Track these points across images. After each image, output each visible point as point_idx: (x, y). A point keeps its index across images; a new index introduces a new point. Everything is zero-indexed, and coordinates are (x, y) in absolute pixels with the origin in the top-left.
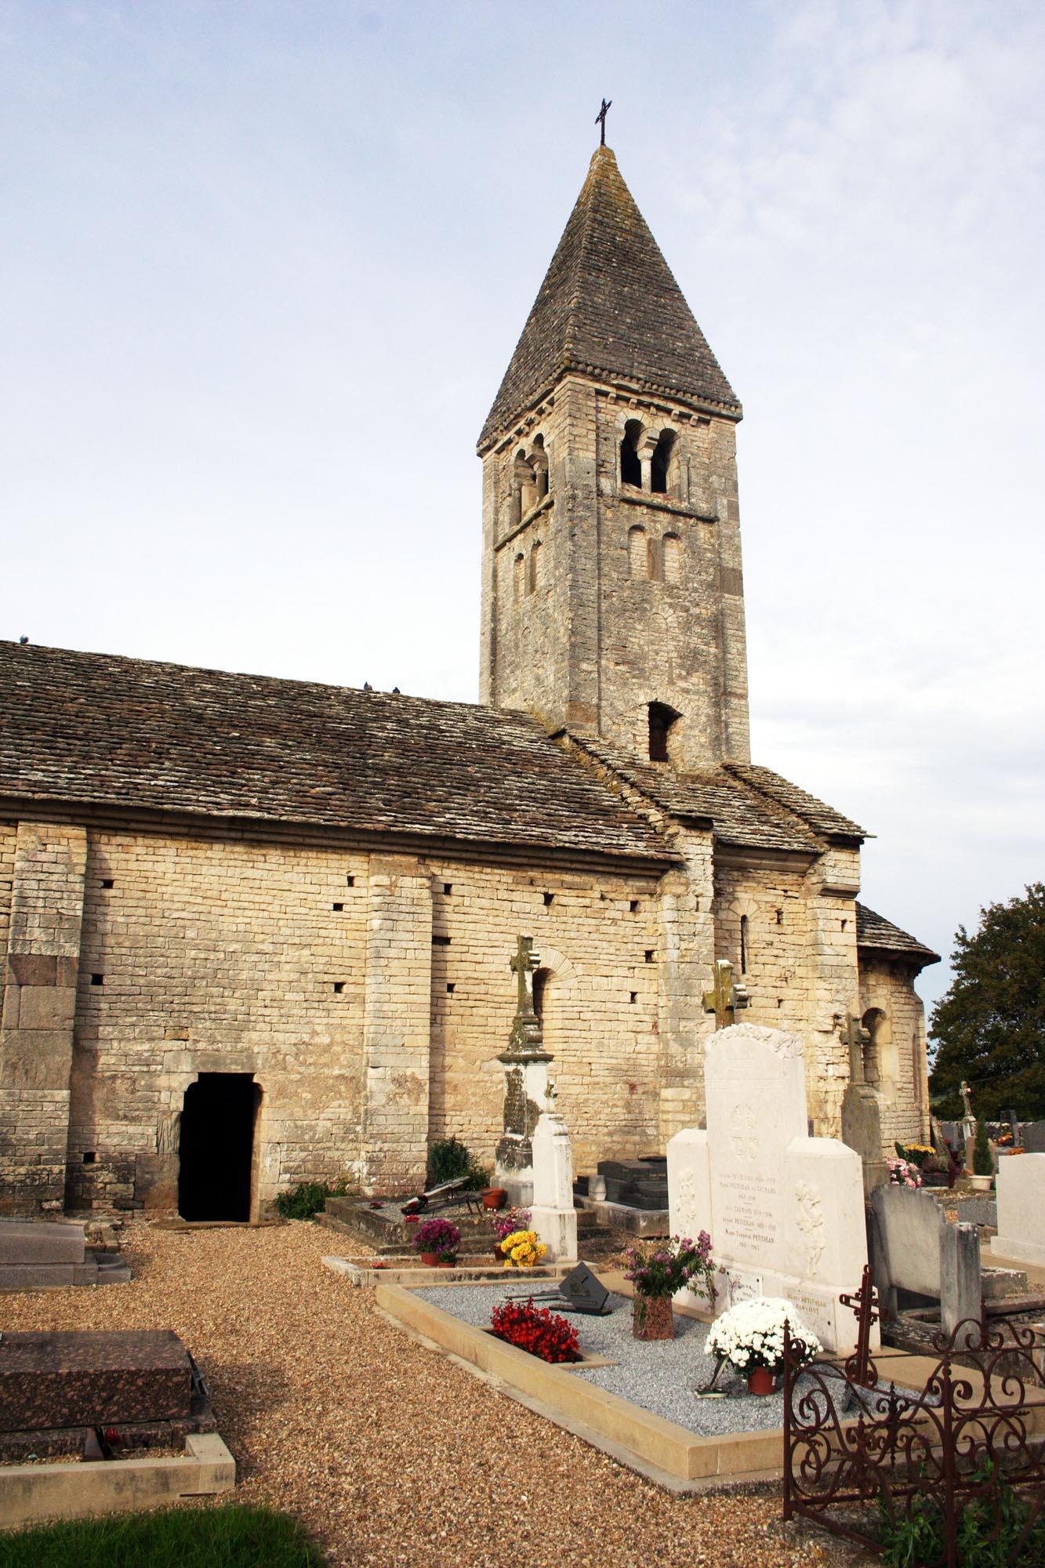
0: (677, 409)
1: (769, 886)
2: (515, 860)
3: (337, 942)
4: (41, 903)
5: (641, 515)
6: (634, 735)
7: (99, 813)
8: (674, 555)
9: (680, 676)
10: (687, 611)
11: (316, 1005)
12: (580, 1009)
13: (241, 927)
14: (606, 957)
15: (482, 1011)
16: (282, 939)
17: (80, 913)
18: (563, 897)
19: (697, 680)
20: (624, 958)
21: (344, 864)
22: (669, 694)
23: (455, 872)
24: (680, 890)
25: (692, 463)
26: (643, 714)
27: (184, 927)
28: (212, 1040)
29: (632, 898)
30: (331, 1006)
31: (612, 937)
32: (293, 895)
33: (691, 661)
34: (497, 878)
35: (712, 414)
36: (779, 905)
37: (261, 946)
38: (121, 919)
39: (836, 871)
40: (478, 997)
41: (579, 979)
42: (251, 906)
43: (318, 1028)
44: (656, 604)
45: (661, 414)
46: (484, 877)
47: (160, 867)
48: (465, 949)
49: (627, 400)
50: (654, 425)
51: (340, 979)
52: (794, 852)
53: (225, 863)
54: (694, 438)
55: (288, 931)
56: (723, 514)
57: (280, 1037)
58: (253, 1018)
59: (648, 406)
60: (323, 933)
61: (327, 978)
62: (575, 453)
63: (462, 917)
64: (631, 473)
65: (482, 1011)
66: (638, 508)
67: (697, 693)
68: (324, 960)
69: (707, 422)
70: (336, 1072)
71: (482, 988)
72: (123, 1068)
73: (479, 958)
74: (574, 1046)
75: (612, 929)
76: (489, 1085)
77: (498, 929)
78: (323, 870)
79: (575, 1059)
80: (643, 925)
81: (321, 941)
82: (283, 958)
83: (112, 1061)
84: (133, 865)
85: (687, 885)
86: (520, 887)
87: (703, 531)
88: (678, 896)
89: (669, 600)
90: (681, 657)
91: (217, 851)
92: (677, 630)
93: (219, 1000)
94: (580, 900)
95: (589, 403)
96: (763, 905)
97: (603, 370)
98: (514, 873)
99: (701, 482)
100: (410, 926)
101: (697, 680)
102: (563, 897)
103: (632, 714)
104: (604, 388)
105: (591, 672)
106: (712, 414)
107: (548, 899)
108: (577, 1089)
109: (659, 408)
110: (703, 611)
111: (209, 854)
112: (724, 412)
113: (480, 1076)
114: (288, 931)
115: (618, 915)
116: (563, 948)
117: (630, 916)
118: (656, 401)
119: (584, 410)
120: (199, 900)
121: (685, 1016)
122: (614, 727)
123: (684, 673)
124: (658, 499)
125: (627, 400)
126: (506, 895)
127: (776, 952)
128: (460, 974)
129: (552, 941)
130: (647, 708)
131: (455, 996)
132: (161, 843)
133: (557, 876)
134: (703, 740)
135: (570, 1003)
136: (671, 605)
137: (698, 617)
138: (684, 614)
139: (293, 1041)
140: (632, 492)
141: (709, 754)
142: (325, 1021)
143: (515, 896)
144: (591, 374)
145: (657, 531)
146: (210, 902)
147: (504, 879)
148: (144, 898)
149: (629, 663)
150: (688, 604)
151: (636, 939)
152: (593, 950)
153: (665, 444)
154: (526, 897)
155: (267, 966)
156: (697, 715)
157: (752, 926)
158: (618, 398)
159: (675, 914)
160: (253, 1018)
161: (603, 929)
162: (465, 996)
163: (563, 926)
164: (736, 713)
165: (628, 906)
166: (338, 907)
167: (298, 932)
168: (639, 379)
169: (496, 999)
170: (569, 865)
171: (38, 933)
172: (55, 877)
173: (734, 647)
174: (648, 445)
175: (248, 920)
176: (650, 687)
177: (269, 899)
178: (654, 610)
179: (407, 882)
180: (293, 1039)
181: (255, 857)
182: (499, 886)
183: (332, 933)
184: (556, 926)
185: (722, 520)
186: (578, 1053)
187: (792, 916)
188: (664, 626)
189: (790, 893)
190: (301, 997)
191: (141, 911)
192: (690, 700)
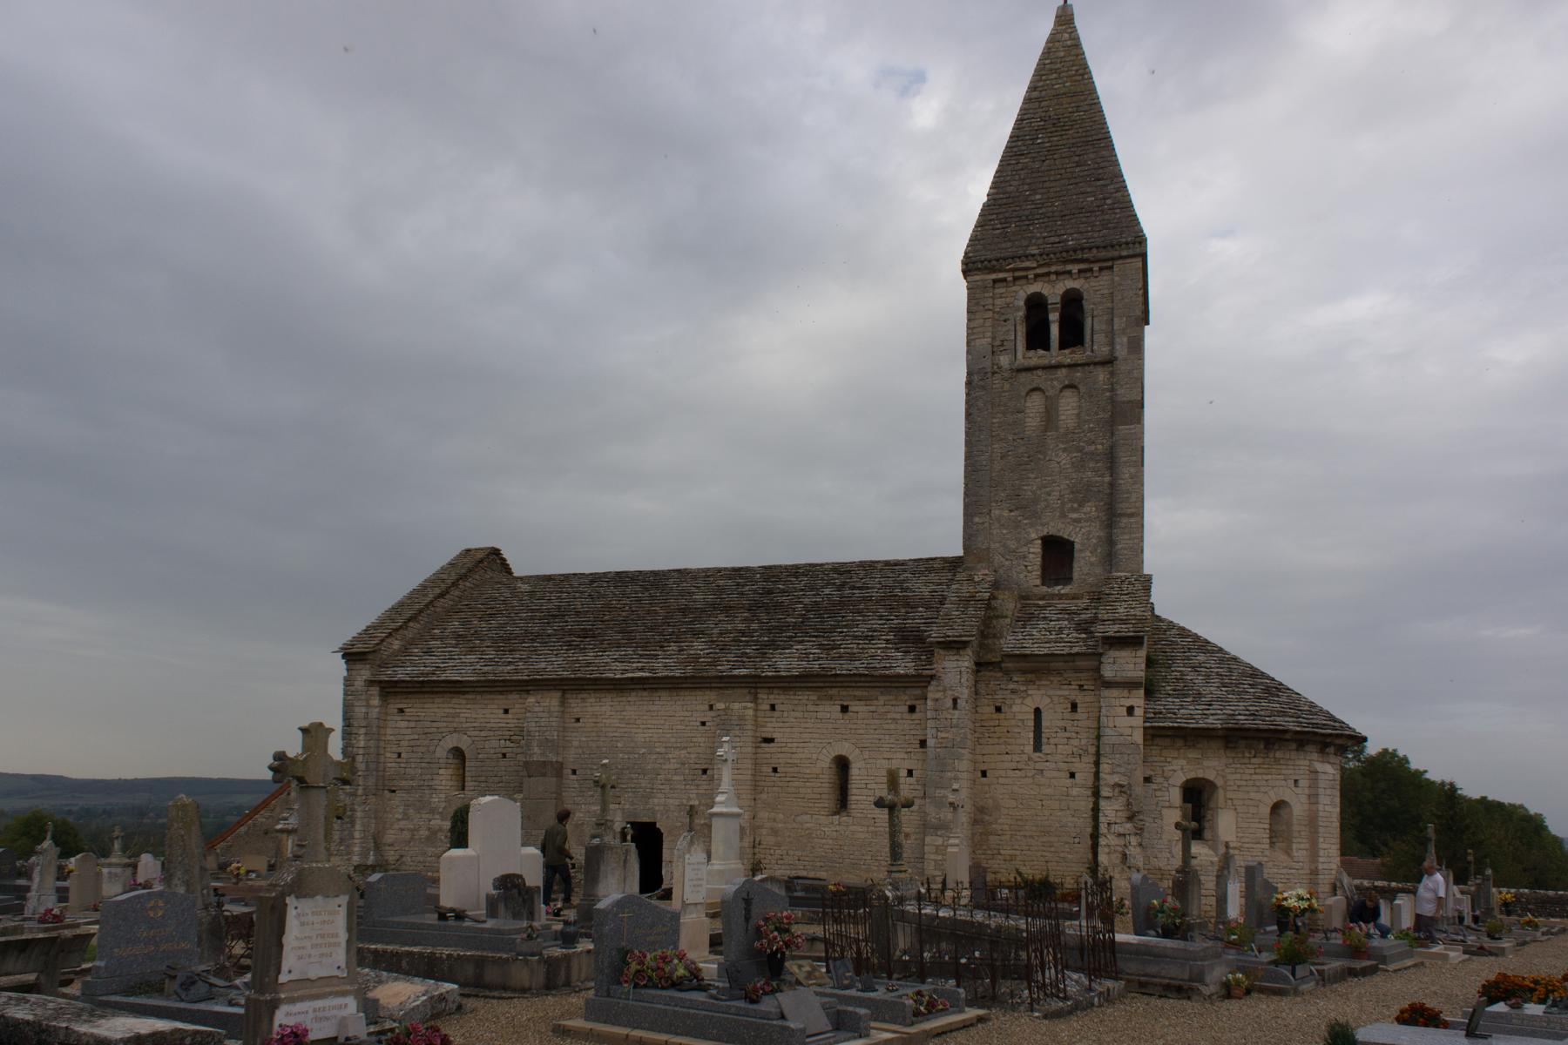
0: (1075, 268)
1: (1064, 682)
2: (815, 685)
3: (701, 745)
4: (537, 734)
5: (1039, 378)
6: (1026, 566)
7: (598, 682)
8: (1068, 406)
9: (1073, 510)
10: (1080, 451)
11: (690, 782)
12: (867, 782)
13: (648, 739)
14: (887, 745)
15: (796, 784)
16: (670, 745)
17: (555, 738)
18: (855, 707)
19: (1090, 509)
20: (902, 746)
21: (707, 697)
22: (1061, 526)
23: (777, 697)
24: (938, 695)
25: (1095, 313)
26: (1037, 548)
27: (617, 741)
28: (633, 804)
29: (909, 703)
30: (699, 783)
31: (892, 732)
32: (675, 718)
33: (1081, 494)
34: (806, 697)
35: (1113, 259)
36: (1072, 698)
37: (658, 750)
38: (584, 739)
39: (1116, 667)
40: (792, 775)
41: (866, 761)
42: (653, 726)
43: (691, 796)
44: (1050, 452)
45: (1061, 277)
46: (797, 697)
47: (604, 709)
48: (784, 744)
49: (1026, 277)
50: (1053, 292)
51: (705, 767)
52: (1077, 654)
53: (637, 703)
54: (1094, 289)
55: (674, 740)
56: (1121, 351)
57: (671, 801)
58: (655, 791)
59: (1048, 274)
60: (694, 739)
61: (697, 766)
62: (973, 344)
63: (781, 724)
64: (1037, 338)
65: (796, 784)
66: (1035, 372)
67: (1089, 520)
68: (695, 755)
69: (1111, 268)
70: (702, 822)
71: (797, 769)
72: (587, 819)
73: (794, 750)
74: (862, 806)
75: (892, 726)
76: (800, 831)
77: (808, 730)
78: (694, 702)
79: (862, 815)
80: (919, 722)
81: (692, 745)
82: (670, 756)
83: (582, 815)
84: (590, 709)
85: (944, 691)
86: (823, 702)
87: (1101, 375)
88: (937, 700)
89: (1062, 446)
90: (1073, 493)
91: (633, 697)
92: (1070, 470)
93: (636, 781)
94: (868, 707)
95: (986, 295)
96: (1056, 699)
97: (997, 260)
98: (819, 693)
99: (1104, 327)
100: (737, 733)
101: (1090, 509)
102: (855, 707)
103: (1025, 549)
104: (1001, 275)
105: (983, 523)
106: (1113, 259)
107: (845, 709)
108: (862, 836)
109: (1057, 273)
110: (1100, 447)
111: (629, 699)
112: (1124, 253)
113: (794, 825)
114: (674, 740)
115: (898, 716)
116: (854, 741)
117: (907, 716)
118: (1053, 269)
119: (982, 303)
120: (623, 725)
121: (939, 785)
122: (1007, 563)
123: (1076, 505)
124: (1068, 356)
125: (1026, 277)
126: (812, 708)
127: (1067, 735)
128: (781, 761)
129: (845, 737)
130: (1040, 542)
131: (777, 775)
132: (603, 695)
133: (851, 693)
134: (1093, 559)
135: (858, 778)
136: (1065, 450)
137: (1092, 453)
138: (1079, 454)
139: (677, 804)
140: (1038, 357)
141: (1098, 570)
142: (696, 791)
143: (820, 708)
144: (986, 268)
145: (1053, 387)
146: (631, 726)
147: (811, 698)
148: (596, 727)
149: (1021, 508)
150: (1082, 444)
151: (912, 732)
152: (877, 741)
153: (1072, 302)
154: (828, 708)
155: (661, 761)
156: (1088, 539)
157: (1045, 715)
158: (1015, 279)
159: (934, 713)
160: (655, 791)
161: (886, 726)
162: (784, 775)
163: (855, 726)
164: (1126, 531)
165: (906, 709)
166: (703, 724)
167: (679, 740)
168: (1033, 255)
169: (805, 776)
170: (854, 684)
171: (536, 749)
172: (543, 720)
173: (1125, 473)
174: (1054, 310)
175: (650, 735)
176: (1042, 525)
177: (662, 722)
178: (1047, 458)
179: (736, 706)
180: (677, 802)
181: (654, 699)
182: (808, 703)
183: (700, 740)
184: (850, 726)
185: (1120, 358)
186: (865, 811)
187: (1085, 705)
188: (1057, 470)
189: (1085, 687)
190: (682, 778)
191: (594, 734)
192: (1082, 527)
